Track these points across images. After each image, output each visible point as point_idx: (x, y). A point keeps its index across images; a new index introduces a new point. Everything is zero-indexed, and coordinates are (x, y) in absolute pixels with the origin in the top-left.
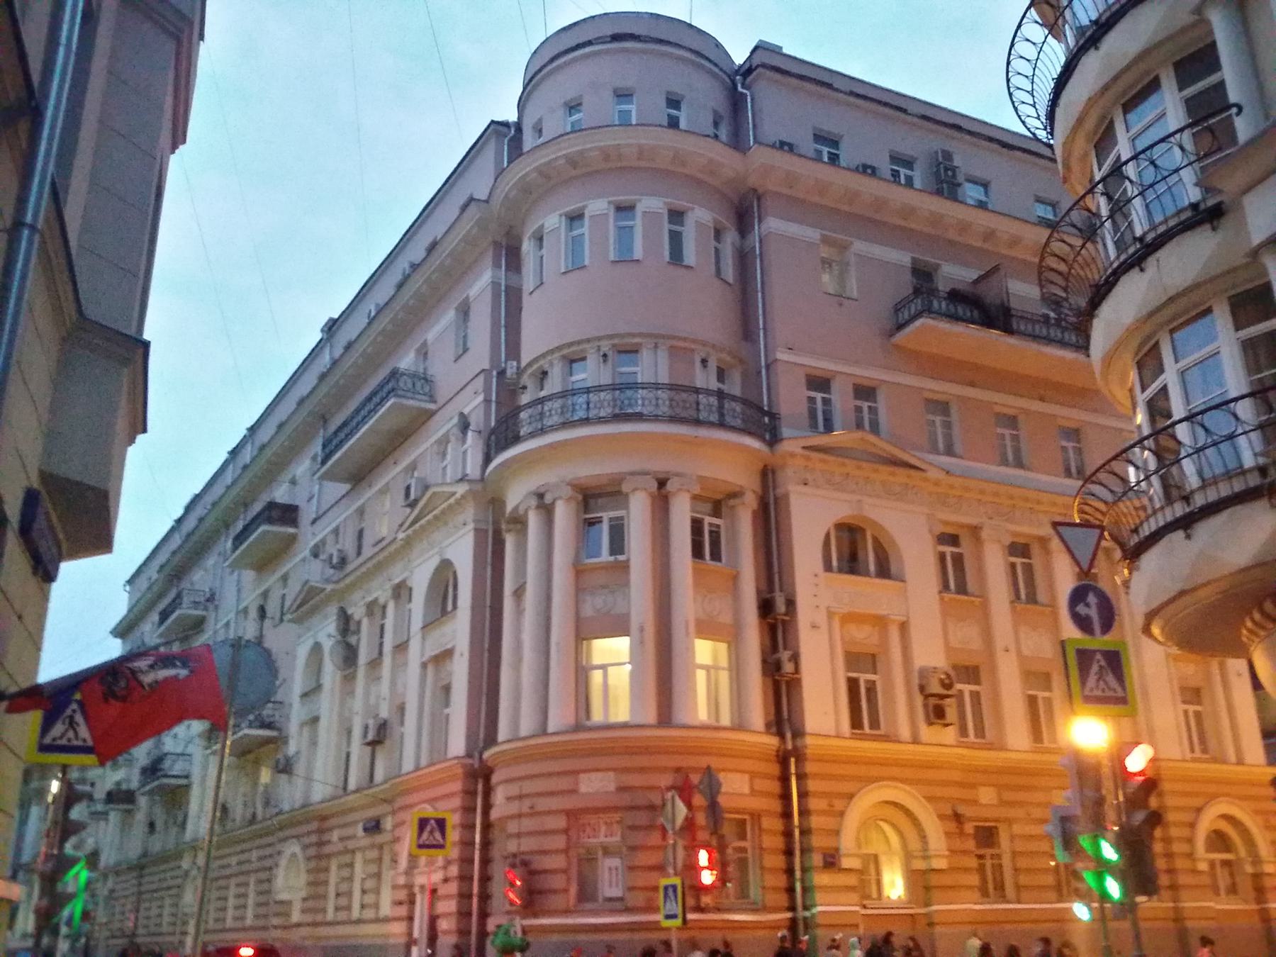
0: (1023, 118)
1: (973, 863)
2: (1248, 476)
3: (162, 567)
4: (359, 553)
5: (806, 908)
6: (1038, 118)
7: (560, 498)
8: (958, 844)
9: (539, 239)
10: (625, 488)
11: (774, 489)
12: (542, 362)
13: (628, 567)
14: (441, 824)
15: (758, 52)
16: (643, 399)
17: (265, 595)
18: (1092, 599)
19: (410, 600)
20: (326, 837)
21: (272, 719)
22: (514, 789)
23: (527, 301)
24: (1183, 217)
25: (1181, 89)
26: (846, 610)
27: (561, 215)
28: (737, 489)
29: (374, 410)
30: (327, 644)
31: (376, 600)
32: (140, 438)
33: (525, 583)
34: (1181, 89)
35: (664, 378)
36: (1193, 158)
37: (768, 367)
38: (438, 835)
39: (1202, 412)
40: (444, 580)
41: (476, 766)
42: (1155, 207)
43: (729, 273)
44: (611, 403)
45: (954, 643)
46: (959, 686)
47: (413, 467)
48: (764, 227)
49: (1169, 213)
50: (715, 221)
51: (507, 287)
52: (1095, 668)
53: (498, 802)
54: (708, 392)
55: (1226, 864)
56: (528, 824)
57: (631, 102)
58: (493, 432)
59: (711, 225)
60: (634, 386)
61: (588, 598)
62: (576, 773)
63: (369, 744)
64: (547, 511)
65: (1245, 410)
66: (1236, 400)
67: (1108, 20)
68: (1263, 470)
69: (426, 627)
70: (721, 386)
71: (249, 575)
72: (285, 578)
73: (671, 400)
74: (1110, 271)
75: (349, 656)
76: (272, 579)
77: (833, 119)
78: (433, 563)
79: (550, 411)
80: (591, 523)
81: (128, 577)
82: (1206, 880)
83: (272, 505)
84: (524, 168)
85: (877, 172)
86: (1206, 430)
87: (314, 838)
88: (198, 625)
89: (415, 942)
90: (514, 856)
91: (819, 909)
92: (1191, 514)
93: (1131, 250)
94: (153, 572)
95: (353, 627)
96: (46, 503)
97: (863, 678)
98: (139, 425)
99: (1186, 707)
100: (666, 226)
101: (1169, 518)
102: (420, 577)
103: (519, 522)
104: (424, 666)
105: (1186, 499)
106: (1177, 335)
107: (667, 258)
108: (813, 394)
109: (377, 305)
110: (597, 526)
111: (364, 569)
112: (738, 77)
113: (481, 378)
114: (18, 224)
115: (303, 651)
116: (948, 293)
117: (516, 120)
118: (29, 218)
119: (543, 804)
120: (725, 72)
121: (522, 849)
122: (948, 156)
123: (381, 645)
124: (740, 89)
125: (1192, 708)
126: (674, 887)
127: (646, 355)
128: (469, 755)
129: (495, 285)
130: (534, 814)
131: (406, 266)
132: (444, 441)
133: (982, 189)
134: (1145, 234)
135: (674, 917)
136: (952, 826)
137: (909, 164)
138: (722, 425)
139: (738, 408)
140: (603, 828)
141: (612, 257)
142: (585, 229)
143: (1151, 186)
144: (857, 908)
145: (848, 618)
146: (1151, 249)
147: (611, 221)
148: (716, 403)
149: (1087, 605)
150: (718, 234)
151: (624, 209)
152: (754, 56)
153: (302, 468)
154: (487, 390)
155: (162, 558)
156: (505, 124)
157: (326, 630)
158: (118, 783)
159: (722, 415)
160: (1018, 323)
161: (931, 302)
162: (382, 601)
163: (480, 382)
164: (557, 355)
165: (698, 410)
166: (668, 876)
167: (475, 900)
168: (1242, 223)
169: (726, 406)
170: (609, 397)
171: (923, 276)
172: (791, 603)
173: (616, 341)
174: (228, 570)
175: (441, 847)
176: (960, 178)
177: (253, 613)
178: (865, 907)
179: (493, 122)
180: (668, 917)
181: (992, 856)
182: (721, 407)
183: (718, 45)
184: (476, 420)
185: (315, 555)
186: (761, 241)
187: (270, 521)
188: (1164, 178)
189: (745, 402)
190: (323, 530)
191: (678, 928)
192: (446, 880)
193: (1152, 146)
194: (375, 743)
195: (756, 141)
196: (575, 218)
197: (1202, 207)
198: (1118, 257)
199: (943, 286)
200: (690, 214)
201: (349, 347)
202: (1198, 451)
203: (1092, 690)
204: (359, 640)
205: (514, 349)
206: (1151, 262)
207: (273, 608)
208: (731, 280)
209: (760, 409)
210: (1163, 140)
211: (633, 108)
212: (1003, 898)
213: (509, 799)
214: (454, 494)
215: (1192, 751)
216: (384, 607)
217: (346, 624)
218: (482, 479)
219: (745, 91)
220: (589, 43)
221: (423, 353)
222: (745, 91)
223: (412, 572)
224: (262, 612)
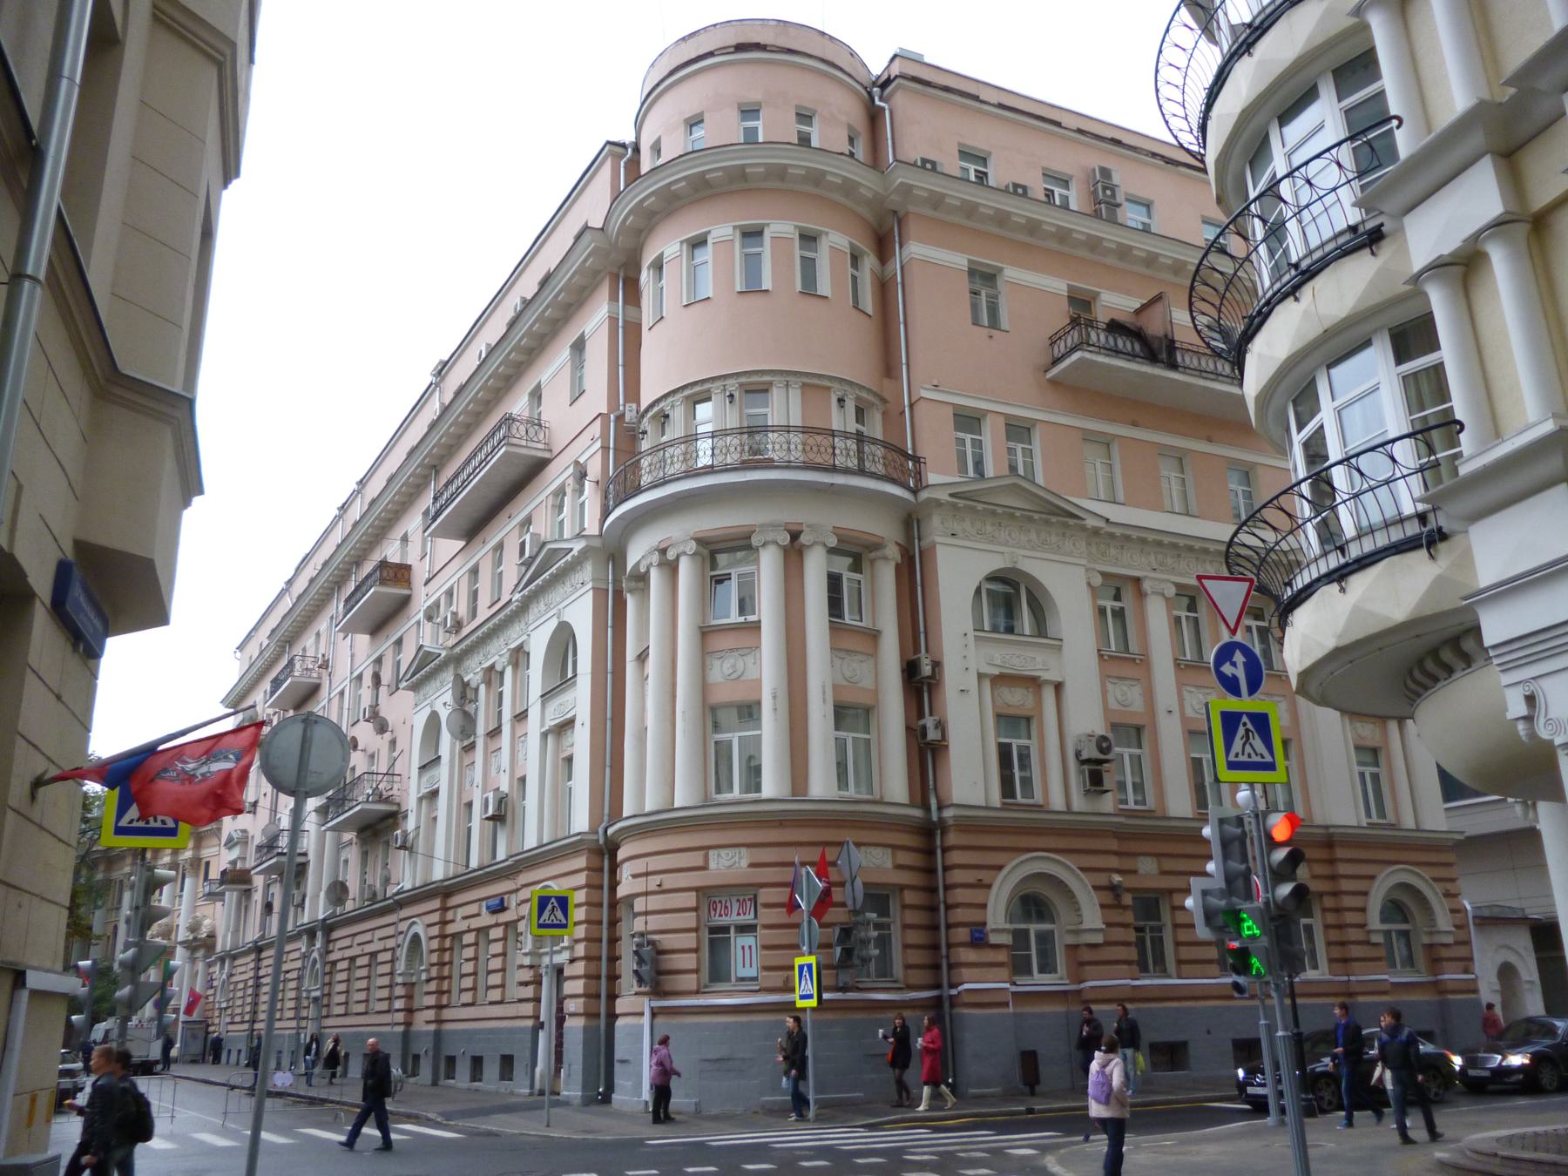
0: (1175, 132)
1: (1131, 936)
2: (1407, 525)
3: (273, 631)
4: (474, 615)
5: (952, 986)
6: (1191, 132)
7: (684, 553)
8: (1116, 916)
9: (658, 266)
10: (755, 541)
11: (919, 540)
12: (662, 405)
13: (760, 627)
14: (563, 902)
15: (897, 61)
16: (774, 443)
17: (379, 661)
18: (1239, 658)
19: (528, 668)
20: (450, 915)
21: (390, 793)
22: (639, 866)
23: (647, 337)
24: (1341, 240)
25: (1339, 101)
26: (996, 671)
27: (682, 242)
28: (875, 540)
29: (485, 461)
30: (444, 714)
31: (492, 667)
32: (196, 500)
33: (648, 647)
34: (1339, 101)
35: (796, 420)
36: (1351, 176)
37: (911, 406)
38: (559, 914)
39: (1357, 455)
40: (564, 639)
41: (601, 841)
42: (1311, 231)
43: (868, 302)
44: (738, 449)
45: (1113, 705)
46: (1117, 750)
47: (528, 521)
48: (905, 253)
49: (1325, 238)
50: (852, 246)
51: (625, 322)
52: (1241, 731)
53: (624, 880)
54: (845, 435)
55: (1405, 934)
56: (655, 902)
57: (758, 119)
58: (611, 481)
59: (848, 251)
60: (765, 429)
61: (717, 663)
62: (706, 848)
63: (488, 819)
64: (671, 568)
65: (1405, 452)
66: (1393, 441)
67: (1262, 23)
68: (1422, 518)
69: (546, 696)
70: (860, 427)
71: (363, 640)
72: (399, 642)
73: (804, 444)
74: (1263, 301)
75: (465, 725)
76: (386, 645)
77: (981, 134)
78: (553, 624)
79: (672, 457)
80: (720, 580)
81: (237, 645)
82: (1382, 952)
83: (383, 564)
84: (643, 192)
85: (1029, 191)
86: (1362, 474)
87: (435, 917)
88: (314, 690)
89: (542, 1025)
90: (642, 935)
91: (967, 986)
92: (1347, 565)
93: (1286, 278)
94: (263, 636)
95: (470, 695)
96: (77, 574)
97: (1015, 743)
98: (191, 484)
99: (1362, 769)
100: (797, 253)
101: (1324, 570)
102: (538, 638)
103: (642, 578)
104: (544, 735)
105: (1342, 549)
106: (1333, 371)
107: (799, 287)
108: (961, 435)
109: (488, 345)
110: (726, 583)
111: (479, 633)
112: (875, 89)
113: (598, 422)
114: (17, 276)
115: (420, 720)
116: (1108, 325)
117: (634, 140)
118: (29, 271)
119: (670, 881)
120: (861, 84)
121: (650, 928)
122: (1106, 173)
123: (500, 713)
124: (877, 102)
125: (1368, 770)
126: (810, 966)
127: (776, 395)
128: (593, 831)
129: (613, 320)
130: (661, 891)
131: (518, 301)
132: (560, 492)
133: (1144, 209)
134: (1300, 260)
135: (810, 997)
136: (1108, 898)
137: (1065, 183)
138: (861, 472)
139: (879, 451)
140: (736, 907)
141: (738, 289)
142: (706, 255)
143: (1307, 206)
144: (1007, 985)
145: (1002, 680)
146: (1307, 275)
147: (737, 245)
148: (854, 447)
149: (1234, 664)
150: (855, 259)
151: (752, 234)
152: (892, 66)
153: (413, 523)
154: (604, 435)
155: (273, 621)
156: (623, 146)
157: (442, 698)
158: (234, 863)
159: (861, 460)
160: (1183, 357)
161: (1088, 335)
162: (499, 668)
163: (596, 428)
164: (679, 396)
165: (834, 454)
166: (803, 955)
167: (604, 981)
168: (1404, 250)
169: (866, 449)
170: (736, 441)
171: (1081, 304)
172: (937, 665)
173: (743, 380)
174: (341, 635)
175: (565, 926)
176: (1120, 198)
177: (367, 680)
178: (1014, 984)
179: (608, 143)
180: (803, 997)
181: (1152, 929)
182: (860, 451)
183: (853, 54)
184: (594, 470)
185: (429, 618)
186: (902, 268)
187: (383, 582)
188: (1320, 198)
189: (886, 445)
190: (437, 590)
191: (813, 1009)
192: (572, 961)
193: (1306, 163)
194: (498, 818)
195: (896, 160)
196: (698, 243)
197: (1361, 229)
198: (1272, 285)
199: (1103, 317)
200: (824, 238)
201: (459, 392)
202: (1356, 496)
203: (1237, 755)
204: (477, 709)
205: (633, 392)
206: (1306, 292)
207: (387, 675)
208: (870, 310)
209: (904, 454)
210: (1318, 156)
211: (759, 124)
212: (1164, 973)
213: (635, 876)
214: (571, 550)
215: (1368, 814)
216: (502, 673)
217: (464, 693)
218: (601, 535)
219: (882, 104)
220: (711, 54)
221: (536, 395)
222: (882, 104)
223: (529, 635)
224: (377, 679)
